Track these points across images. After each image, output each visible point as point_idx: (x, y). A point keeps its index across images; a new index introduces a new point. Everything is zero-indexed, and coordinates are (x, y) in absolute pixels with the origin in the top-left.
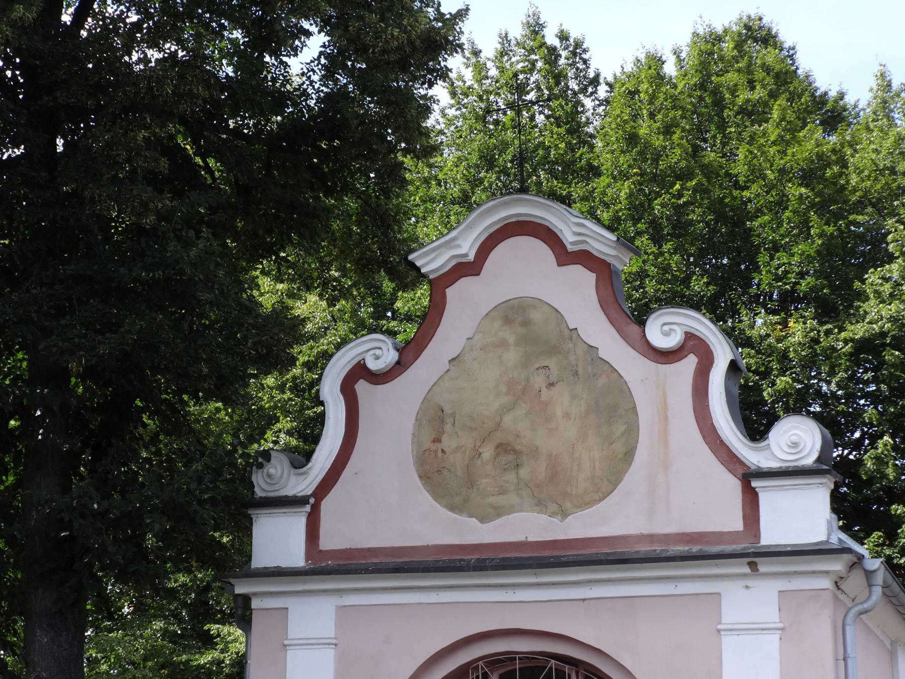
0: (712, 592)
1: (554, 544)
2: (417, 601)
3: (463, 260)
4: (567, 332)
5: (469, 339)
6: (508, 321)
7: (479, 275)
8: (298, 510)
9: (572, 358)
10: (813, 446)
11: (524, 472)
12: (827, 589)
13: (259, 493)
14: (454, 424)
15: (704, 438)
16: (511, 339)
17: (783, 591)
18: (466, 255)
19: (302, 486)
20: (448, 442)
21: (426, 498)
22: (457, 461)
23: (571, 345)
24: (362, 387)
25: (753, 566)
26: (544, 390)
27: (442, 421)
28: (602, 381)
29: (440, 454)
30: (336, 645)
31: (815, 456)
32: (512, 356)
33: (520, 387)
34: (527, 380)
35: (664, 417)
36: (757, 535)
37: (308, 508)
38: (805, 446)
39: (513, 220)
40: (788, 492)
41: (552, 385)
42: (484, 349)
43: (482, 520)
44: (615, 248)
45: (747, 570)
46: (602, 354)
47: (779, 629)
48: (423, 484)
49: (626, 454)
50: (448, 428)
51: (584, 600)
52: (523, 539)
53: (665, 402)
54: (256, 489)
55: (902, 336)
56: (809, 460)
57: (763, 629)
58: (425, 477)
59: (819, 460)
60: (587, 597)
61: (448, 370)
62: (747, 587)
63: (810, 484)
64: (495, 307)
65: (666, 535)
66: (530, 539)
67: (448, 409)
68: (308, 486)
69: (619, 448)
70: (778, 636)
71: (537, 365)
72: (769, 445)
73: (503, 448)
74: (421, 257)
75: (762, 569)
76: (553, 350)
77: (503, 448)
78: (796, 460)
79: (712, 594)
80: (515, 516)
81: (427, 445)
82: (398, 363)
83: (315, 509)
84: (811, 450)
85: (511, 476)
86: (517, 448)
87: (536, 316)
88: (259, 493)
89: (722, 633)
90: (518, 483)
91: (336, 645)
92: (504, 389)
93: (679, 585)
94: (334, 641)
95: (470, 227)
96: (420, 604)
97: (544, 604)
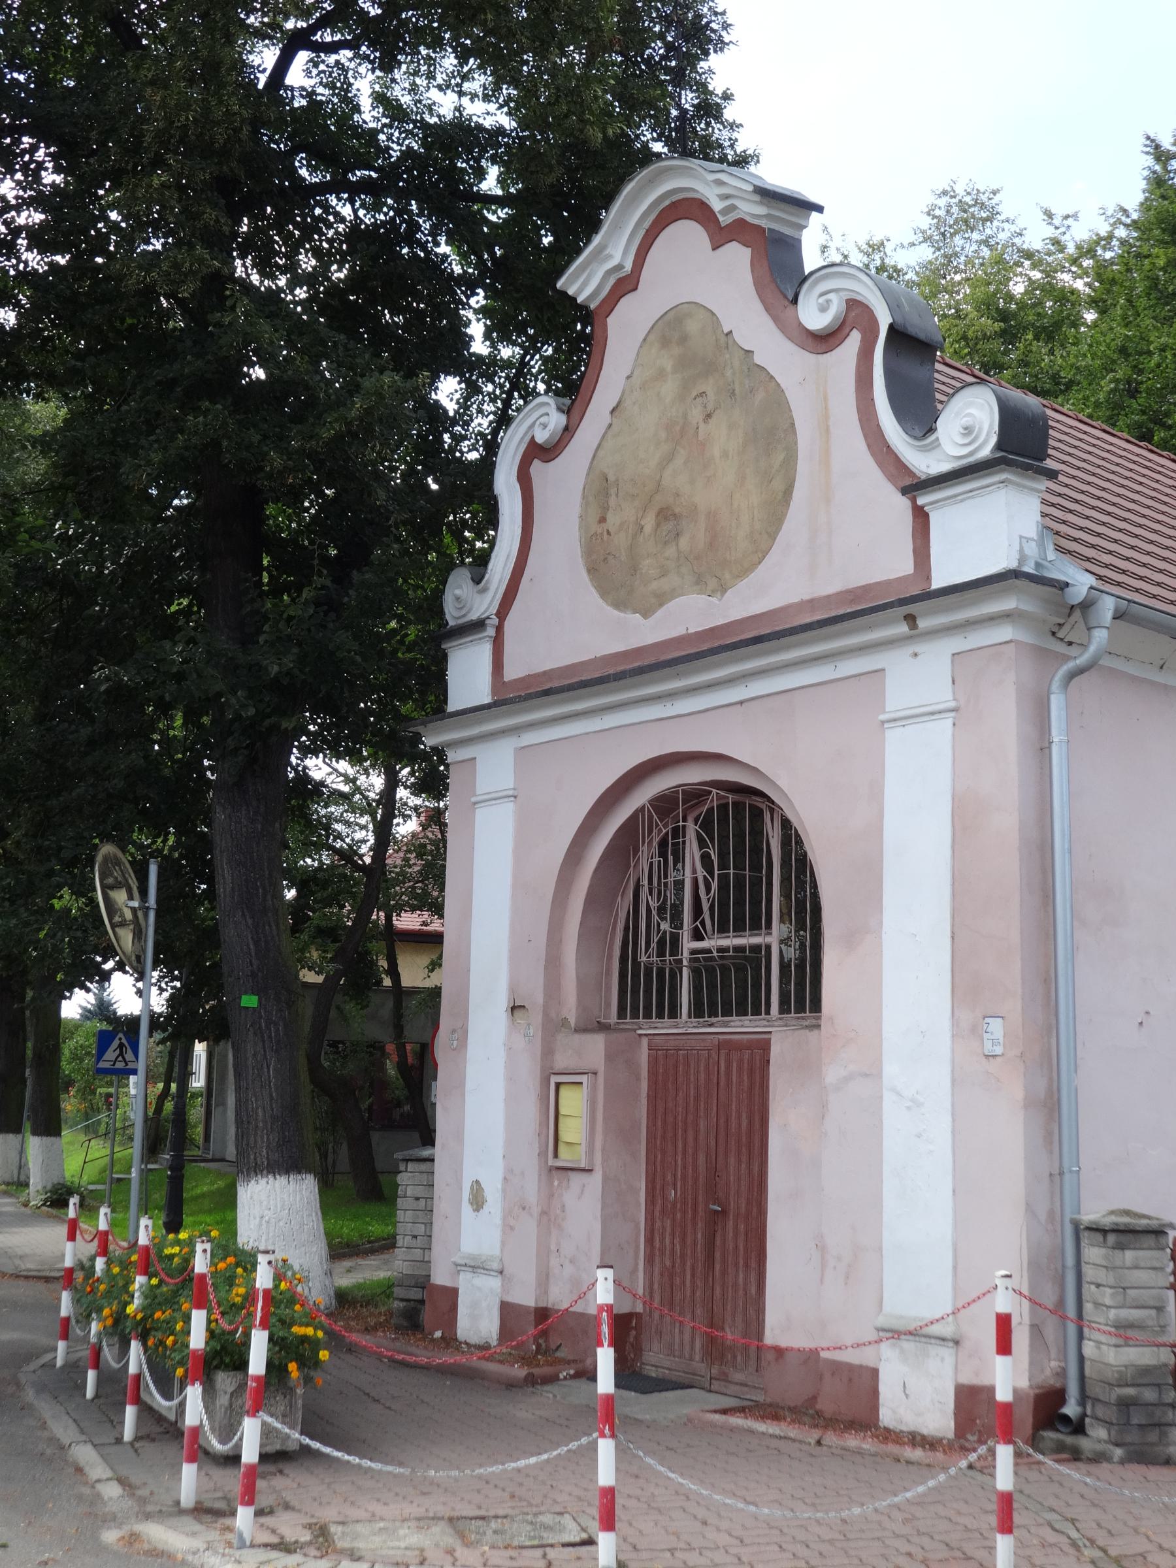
0: (875, 668)
1: (712, 630)
2: (583, 731)
3: (621, 274)
4: (723, 339)
5: (628, 377)
6: (665, 342)
7: (635, 289)
8: (481, 636)
9: (729, 373)
10: (991, 425)
11: (684, 542)
12: (1010, 641)
13: (452, 623)
14: (617, 495)
15: (869, 446)
16: (669, 366)
17: (958, 654)
18: (619, 267)
19: (485, 606)
20: (613, 520)
21: (593, 596)
22: (621, 541)
23: (727, 356)
24: (537, 467)
25: (911, 619)
26: (702, 426)
27: (607, 495)
28: (760, 396)
29: (605, 536)
30: (515, 797)
31: (994, 440)
32: (669, 388)
33: (678, 428)
34: (685, 416)
35: (825, 431)
36: (928, 578)
37: (491, 632)
38: (980, 429)
39: (667, 203)
40: (963, 504)
41: (709, 416)
42: (644, 387)
43: (646, 614)
44: (761, 203)
45: (903, 628)
46: (758, 359)
47: (952, 711)
48: (591, 580)
49: (785, 493)
50: (612, 501)
51: (741, 703)
52: (684, 632)
53: (826, 408)
54: (448, 617)
55: (538, 99)
56: (986, 452)
57: (932, 713)
58: (592, 570)
59: (999, 446)
60: (742, 698)
61: (610, 425)
62: (916, 655)
63: (988, 486)
64: (653, 327)
65: (828, 597)
66: (691, 631)
67: (611, 478)
68: (490, 604)
69: (778, 485)
70: (950, 722)
71: (694, 394)
72: (937, 439)
73: (665, 515)
74: (571, 281)
75: (923, 624)
76: (709, 368)
77: (665, 515)
78: (971, 453)
79: (876, 671)
80: (673, 605)
81: (595, 528)
82: (566, 429)
83: (499, 629)
84: (988, 434)
85: (671, 551)
86: (677, 510)
87: (692, 326)
88: (452, 623)
89: (886, 725)
90: (678, 559)
91: (515, 797)
92: (663, 435)
93: (839, 665)
94: (511, 793)
95: (617, 226)
96: (587, 734)
97: (702, 715)
